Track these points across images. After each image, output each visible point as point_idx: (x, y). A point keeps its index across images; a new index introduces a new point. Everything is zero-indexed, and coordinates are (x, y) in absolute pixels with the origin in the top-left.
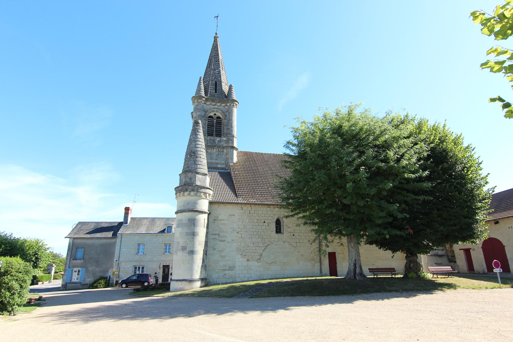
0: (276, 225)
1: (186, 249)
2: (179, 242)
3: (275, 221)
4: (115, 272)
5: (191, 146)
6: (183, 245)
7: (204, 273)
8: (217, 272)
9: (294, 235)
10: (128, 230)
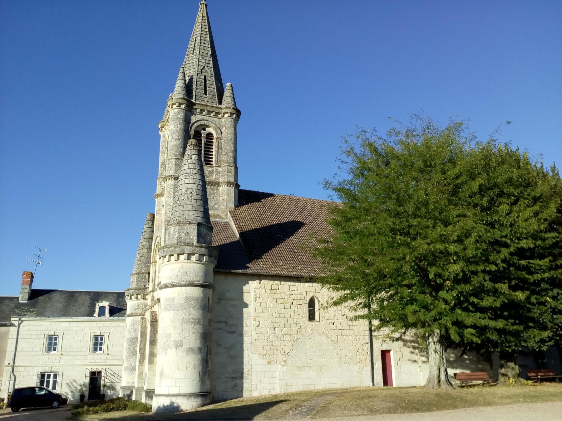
1: (182, 346)
2: (170, 334)
3: (307, 302)
5: (186, 182)
6: (177, 340)
7: (208, 382)
10: (31, 312)
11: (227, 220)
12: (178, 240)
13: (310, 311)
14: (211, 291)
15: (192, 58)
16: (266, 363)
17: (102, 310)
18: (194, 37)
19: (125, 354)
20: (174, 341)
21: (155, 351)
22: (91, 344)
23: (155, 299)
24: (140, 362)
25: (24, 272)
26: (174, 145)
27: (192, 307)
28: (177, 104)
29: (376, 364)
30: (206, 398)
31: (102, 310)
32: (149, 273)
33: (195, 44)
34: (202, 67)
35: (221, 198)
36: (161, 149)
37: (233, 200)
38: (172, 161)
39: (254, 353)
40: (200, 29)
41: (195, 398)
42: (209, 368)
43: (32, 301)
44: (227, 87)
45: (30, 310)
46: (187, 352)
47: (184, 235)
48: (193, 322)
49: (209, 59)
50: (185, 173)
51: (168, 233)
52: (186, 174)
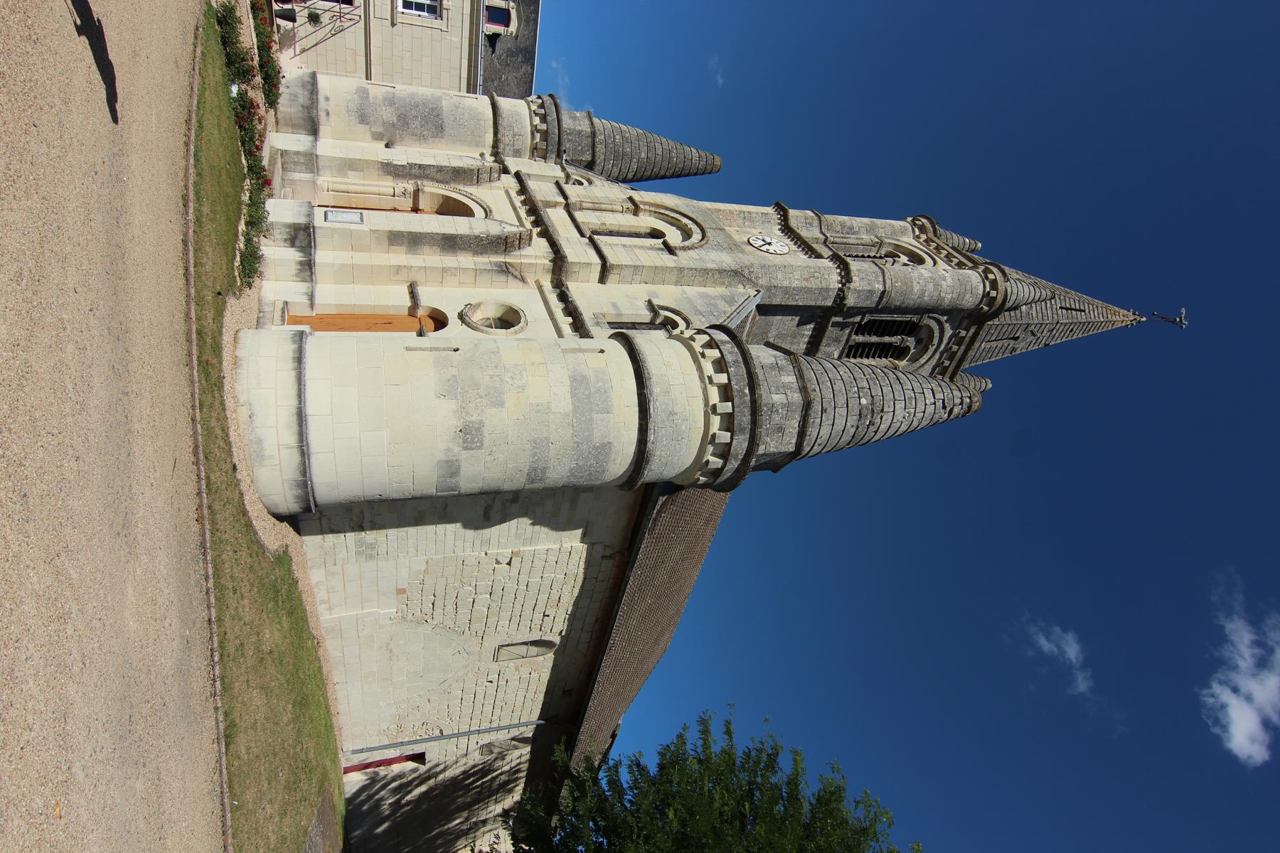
1: (466, 448)
2: (500, 404)
6: (486, 431)
15: (1055, 307)
16: (400, 587)
20: (481, 422)
21: (426, 249)
28: (993, 294)
46: (447, 462)
52: (914, 400)
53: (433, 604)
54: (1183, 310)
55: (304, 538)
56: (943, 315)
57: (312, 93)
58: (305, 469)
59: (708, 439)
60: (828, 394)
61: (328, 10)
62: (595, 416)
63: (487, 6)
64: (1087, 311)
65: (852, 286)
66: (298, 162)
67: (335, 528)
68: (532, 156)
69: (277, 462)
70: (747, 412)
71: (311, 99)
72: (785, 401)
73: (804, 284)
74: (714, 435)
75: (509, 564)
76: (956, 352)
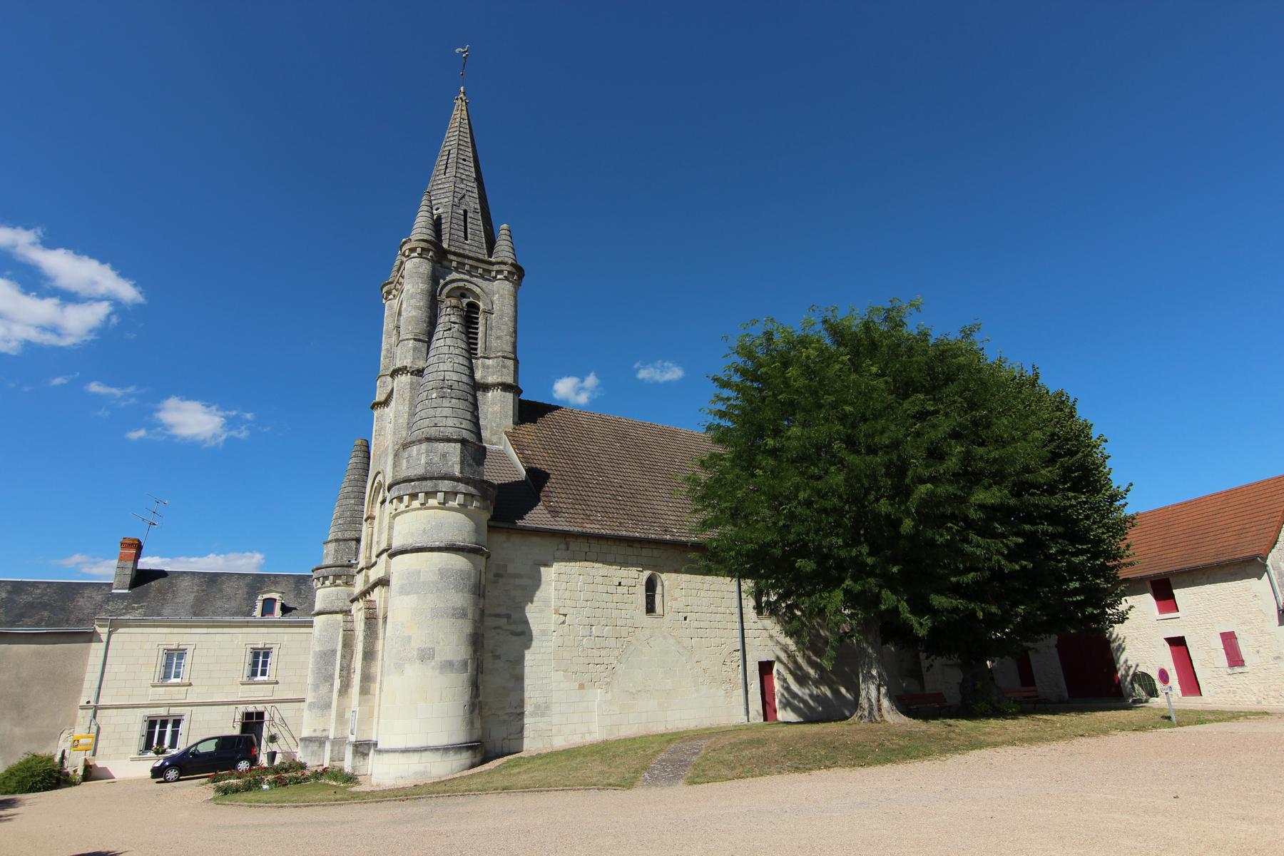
0: (646, 592)
1: (433, 658)
2: (410, 637)
3: (644, 583)
4: (82, 737)
6: (423, 646)
8: (505, 722)
9: (685, 619)
10: (133, 608)
11: (501, 447)
12: (426, 468)
13: (647, 596)
14: (484, 559)
15: (443, 180)
16: (577, 687)
17: (268, 606)
18: (446, 148)
19: (310, 679)
20: (418, 649)
21: (372, 670)
22: (247, 665)
23: (371, 581)
24: (340, 691)
25: (124, 538)
26: (412, 317)
27: (452, 586)
28: (419, 250)
29: (752, 686)
30: (475, 752)
31: (268, 606)
32: (358, 540)
33: (448, 159)
34: (460, 196)
35: (490, 410)
36: (384, 328)
37: (511, 413)
38: (408, 344)
39: (557, 671)
40: (457, 137)
41: (456, 753)
42: (480, 699)
43: (138, 589)
44: (503, 230)
45: (134, 605)
46: (441, 668)
47: (436, 459)
48: (454, 615)
49: (472, 184)
50: (437, 353)
51: (407, 456)
52: (441, 356)
53: (597, 665)
54: (457, 50)
55: (524, 749)
56: (439, 283)
57: (311, 741)
58: (436, 749)
59: (443, 505)
60: (426, 422)
61: (269, 728)
62: (421, 580)
63: (262, 616)
64: (450, 148)
65: (409, 365)
66: (338, 750)
67: (519, 730)
68: (352, 585)
69: (429, 764)
70: (424, 483)
71: (315, 741)
72: (425, 455)
73: (407, 402)
74: (439, 503)
75: (565, 615)
76: (471, 266)
